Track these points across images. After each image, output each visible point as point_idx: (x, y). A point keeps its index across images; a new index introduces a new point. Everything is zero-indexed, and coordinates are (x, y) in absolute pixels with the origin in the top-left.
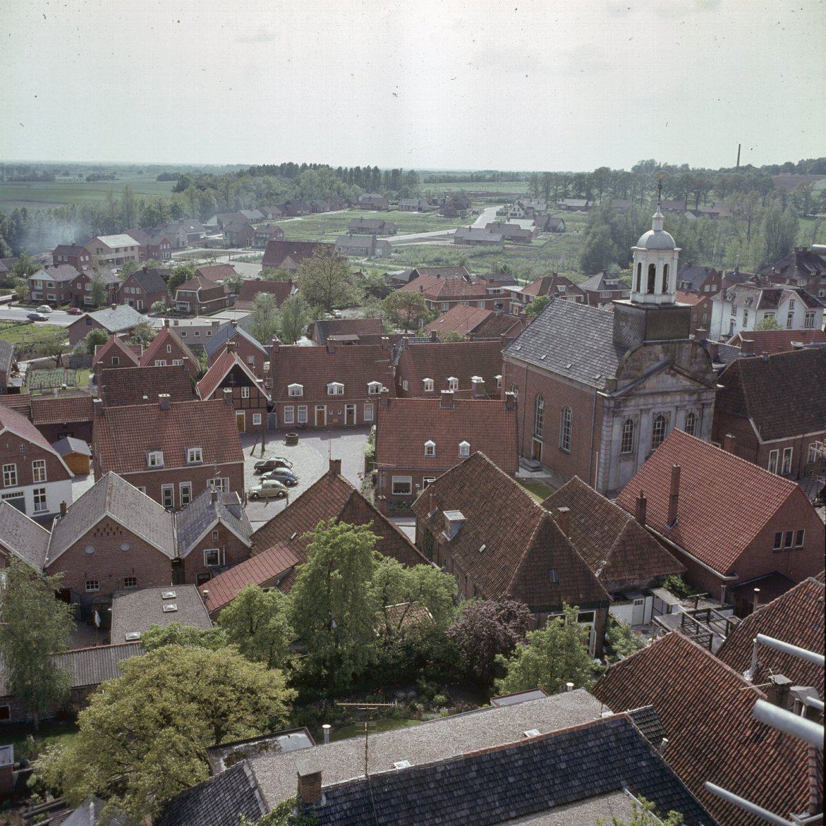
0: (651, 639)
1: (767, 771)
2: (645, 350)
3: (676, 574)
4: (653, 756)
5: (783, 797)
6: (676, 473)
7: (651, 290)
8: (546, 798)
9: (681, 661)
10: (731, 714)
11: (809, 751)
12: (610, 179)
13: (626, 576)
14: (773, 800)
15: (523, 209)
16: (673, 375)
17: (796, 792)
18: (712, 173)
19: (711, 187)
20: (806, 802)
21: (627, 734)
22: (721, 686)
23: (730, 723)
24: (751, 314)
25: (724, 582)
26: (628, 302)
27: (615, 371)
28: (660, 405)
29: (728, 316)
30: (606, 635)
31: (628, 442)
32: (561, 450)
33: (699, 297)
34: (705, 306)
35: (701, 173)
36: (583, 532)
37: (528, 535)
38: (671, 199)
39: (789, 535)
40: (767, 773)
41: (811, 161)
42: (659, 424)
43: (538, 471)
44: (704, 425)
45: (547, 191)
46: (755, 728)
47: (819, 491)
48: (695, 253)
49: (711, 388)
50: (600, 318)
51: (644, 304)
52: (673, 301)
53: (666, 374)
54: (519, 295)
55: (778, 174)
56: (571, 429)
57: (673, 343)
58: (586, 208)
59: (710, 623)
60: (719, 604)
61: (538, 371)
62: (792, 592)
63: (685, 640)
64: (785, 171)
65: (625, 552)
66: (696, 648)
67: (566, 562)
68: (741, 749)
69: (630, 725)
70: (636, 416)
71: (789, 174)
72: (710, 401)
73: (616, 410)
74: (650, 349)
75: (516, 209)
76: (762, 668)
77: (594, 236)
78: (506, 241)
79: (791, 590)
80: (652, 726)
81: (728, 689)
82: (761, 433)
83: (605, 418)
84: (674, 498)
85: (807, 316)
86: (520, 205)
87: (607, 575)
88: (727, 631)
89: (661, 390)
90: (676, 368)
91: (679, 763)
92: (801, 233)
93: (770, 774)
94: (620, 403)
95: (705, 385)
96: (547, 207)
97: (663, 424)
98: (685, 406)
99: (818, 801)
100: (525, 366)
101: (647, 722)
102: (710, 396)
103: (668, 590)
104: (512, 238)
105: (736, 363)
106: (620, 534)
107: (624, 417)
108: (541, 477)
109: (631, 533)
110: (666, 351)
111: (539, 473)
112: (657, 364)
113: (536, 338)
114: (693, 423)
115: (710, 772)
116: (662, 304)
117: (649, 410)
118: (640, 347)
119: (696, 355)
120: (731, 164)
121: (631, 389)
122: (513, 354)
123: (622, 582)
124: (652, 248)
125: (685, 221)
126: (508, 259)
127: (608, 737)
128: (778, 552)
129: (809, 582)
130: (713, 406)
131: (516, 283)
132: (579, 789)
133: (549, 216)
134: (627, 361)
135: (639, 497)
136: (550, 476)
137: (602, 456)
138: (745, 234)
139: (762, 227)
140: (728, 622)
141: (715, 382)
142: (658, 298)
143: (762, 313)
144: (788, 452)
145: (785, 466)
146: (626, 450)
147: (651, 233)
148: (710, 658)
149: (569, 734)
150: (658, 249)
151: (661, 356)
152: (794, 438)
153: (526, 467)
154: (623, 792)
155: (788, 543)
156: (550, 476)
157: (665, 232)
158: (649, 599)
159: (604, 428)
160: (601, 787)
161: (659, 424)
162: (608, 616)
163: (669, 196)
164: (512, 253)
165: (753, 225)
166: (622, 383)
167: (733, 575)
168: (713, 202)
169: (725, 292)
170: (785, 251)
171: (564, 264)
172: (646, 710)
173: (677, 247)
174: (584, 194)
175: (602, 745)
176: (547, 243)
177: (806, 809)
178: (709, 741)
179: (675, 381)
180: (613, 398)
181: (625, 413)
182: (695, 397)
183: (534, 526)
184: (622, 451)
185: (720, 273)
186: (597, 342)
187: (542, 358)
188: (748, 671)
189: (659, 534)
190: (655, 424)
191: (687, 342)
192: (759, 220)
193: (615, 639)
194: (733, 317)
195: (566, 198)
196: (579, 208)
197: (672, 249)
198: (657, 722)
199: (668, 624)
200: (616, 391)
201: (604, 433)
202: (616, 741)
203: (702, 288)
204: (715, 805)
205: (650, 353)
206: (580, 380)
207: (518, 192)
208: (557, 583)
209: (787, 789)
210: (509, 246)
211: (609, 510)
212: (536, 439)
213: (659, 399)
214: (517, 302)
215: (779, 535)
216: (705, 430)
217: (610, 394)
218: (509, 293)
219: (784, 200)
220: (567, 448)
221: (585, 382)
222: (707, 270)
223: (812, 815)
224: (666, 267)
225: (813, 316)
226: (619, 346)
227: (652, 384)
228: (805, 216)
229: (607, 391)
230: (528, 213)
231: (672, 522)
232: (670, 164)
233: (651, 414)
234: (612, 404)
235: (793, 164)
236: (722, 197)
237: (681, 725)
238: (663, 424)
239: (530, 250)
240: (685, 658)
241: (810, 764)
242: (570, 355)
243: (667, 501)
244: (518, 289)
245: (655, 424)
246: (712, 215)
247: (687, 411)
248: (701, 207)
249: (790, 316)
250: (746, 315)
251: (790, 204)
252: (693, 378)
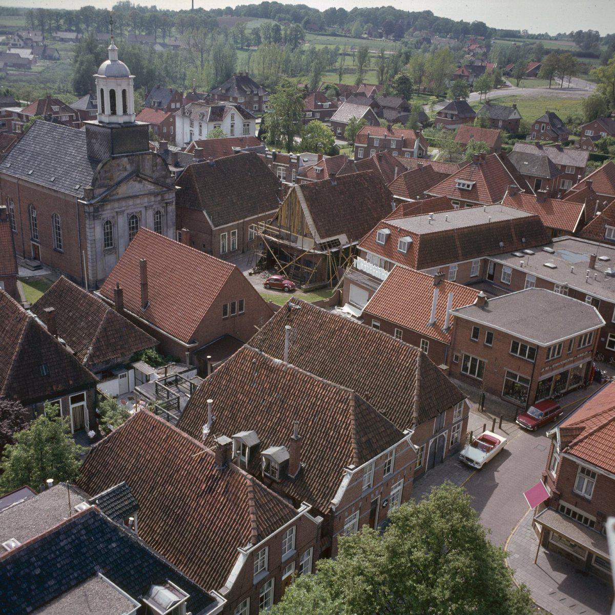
0: (135, 405)
1: (219, 515)
2: (114, 163)
3: (151, 348)
4: (122, 536)
5: (232, 535)
6: (144, 266)
7: (114, 112)
8: (23, 606)
9: (149, 435)
10: (190, 473)
11: (249, 494)
12: (94, 16)
13: (110, 356)
14: (229, 524)
15: (23, 40)
16: (140, 182)
17: (241, 529)
18: (174, 14)
19: (173, 25)
20: (249, 535)
21: (97, 524)
22: (181, 451)
23: (190, 480)
24: (205, 127)
25: (188, 349)
26: (96, 122)
27: (91, 181)
28: (132, 207)
29: (187, 128)
30: (97, 410)
31: (109, 240)
32: (55, 250)
33: (166, 113)
34: (171, 120)
35: (166, 14)
36: (72, 324)
37: (17, 338)
38: (144, 34)
39: (233, 304)
40: (203, 549)
41: (244, 6)
42: (133, 222)
43: (40, 269)
44: (169, 219)
45: (42, 24)
46: (208, 482)
47: (258, 261)
48: (164, 77)
49: (170, 190)
50: (76, 136)
51: (108, 123)
52: (133, 121)
53: (134, 181)
54: (20, 115)
55: (222, 16)
56: (61, 232)
57: (136, 155)
58: (77, 40)
59: (179, 386)
60: (185, 367)
61: (27, 185)
62: (234, 357)
63: (151, 416)
64: (226, 14)
65: (107, 336)
66: (159, 421)
67: (53, 356)
68: (199, 500)
69: (98, 515)
70: (113, 217)
71: (229, 16)
72: (171, 200)
73: (96, 214)
74: (118, 161)
75: (16, 40)
76: (216, 421)
77: (82, 63)
78: (8, 68)
79: (233, 356)
80: (125, 500)
81: (186, 453)
82: (212, 222)
83: (87, 222)
84: (144, 285)
85: (244, 125)
86: (20, 37)
87: (94, 359)
88: (191, 390)
89: (131, 195)
90: (141, 175)
91: (153, 520)
92: (239, 62)
93: (222, 517)
94: (98, 208)
95: (166, 188)
96: (43, 38)
97: (137, 221)
98: (152, 206)
99: (258, 532)
100: (15, 181)
101: (121, 498)
102: (171, 196)
103: (146, 362)
104: (14, 65)
105: (189, 167)
106: (102, 322)
107: (103, 219)
108: (41, 274)
109: (110, 321)
110: (131, 162)
111: (39, 271)
112: (126, 174)
113: (23, 156)
114: (160, 219)
115: (178, 523)
116: (124, 123)
117: (123, 211)
118: (109, 161)
119: (156, 163)
120: (188, 7)
121: (106, 196)
122: (4, 171)
123: (107, 362)
124: (111, 75)
125: (153, 51)
126: (11, 84)
127: (79, 532)
128: (227, 319)
129: (245, 348)
130: (174, 203)
131: (19, 105)
132: (56, 587)
133: (45, 46)
134: (99, 173)
135: (116, 288)
136: (49, 272)
137: (89, 253)
138: (199, 62)
139: (211, 57)
140: (191, 384)
141: (173, 185)
142: (120, 119)
143: (212, 125)
144: (234, 234)
145: (233, 245)
146: (108, 246)
147: (108, 62)
148: (171, 429)
149: (41, 540)
150: (115, 77)
151: (128, 167)
152: (237, 222)
153: (26, 266)
154: (97, 576)
155: (233, 311)
156: (49, 272)
157: (120, 62)
158: (131, 372)
159: (87, 230)
160: (77, 578)
161: (133, 222)
162: (97, 393)
163: (142, 31)
164: (15, 78)
165: (205, 55)
166: (98, 191)
167: (194, 342)
168: (175, 37)
169: (184, 109)
170: (228, 76)
171: (59, 87)
172: (120, 488)
173: (132, 74)
174: (74, 28)
175: (74, 541)
176: (45, 70)
177: (249, 541)
178: (175, 498)
179: (142, 186)
180: (91, 204)
181: (104, 216)
182: (159, 198)
183: (21, 330)
184: (105, 247)
185: (182, 94)
186: (75, 157)
187: (30, 173)
188: (206, 425)
189: (136, 316)
190: (130, 222)
191: (149, 154)
192: (209, 51)
193: (104, 413)
194: (191, 129)
195: (59, 31)
196: (71, 40)
197: (127, 76)
198: (130, 495)
199: (147, 392)
200: (93, 198)
201: (88, 234)
202: (87, 533)
203: (169, 105)
204: (183, 550)
205: (119, 165)
206: (63, 190)
207: (19, 25)
208: (48, 375)
209: (235, 527)
210: (11, 72)
211: (92, 303)
212: (34, 243)
213: (131, 202)
214: (18, 121)
215: (225, 307)
216: (170, 223)
217: (89, 201)
218: (10, 114)
219: (226, 36)
220: (60, 248)
221: (67, 192)
222: (172, 91)
223: (254, 545)
224: (124, 92)
225: (248, 125)
226: (93, 160)
227: (123, 190)
228: (242, 49)
229: (86, 199)
230: (27, 44)
231: (145, 305)
232: (142, 5)
233: (125, 214)
234: (92, 209)
235: (232, 9)
236: (182, 33)
237: (153, 488)
238: (137, 221)
239: (30, 75)
240: (151, 431)
241: (250, 505)
242: (53, 170)
243: (139, 288)
244: (18, 110)
245: (130, 222)
246: (176, 47)
247: (154, 209)
248: (167, 41)
249: (232, 126)
250: (201, 126)
251: (231, 40)
252: (156, 183)
